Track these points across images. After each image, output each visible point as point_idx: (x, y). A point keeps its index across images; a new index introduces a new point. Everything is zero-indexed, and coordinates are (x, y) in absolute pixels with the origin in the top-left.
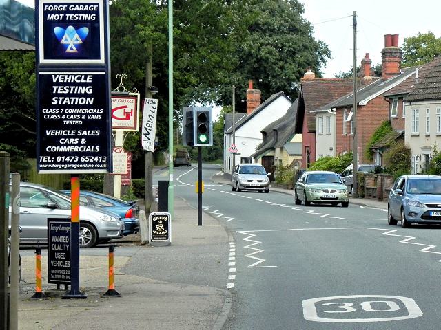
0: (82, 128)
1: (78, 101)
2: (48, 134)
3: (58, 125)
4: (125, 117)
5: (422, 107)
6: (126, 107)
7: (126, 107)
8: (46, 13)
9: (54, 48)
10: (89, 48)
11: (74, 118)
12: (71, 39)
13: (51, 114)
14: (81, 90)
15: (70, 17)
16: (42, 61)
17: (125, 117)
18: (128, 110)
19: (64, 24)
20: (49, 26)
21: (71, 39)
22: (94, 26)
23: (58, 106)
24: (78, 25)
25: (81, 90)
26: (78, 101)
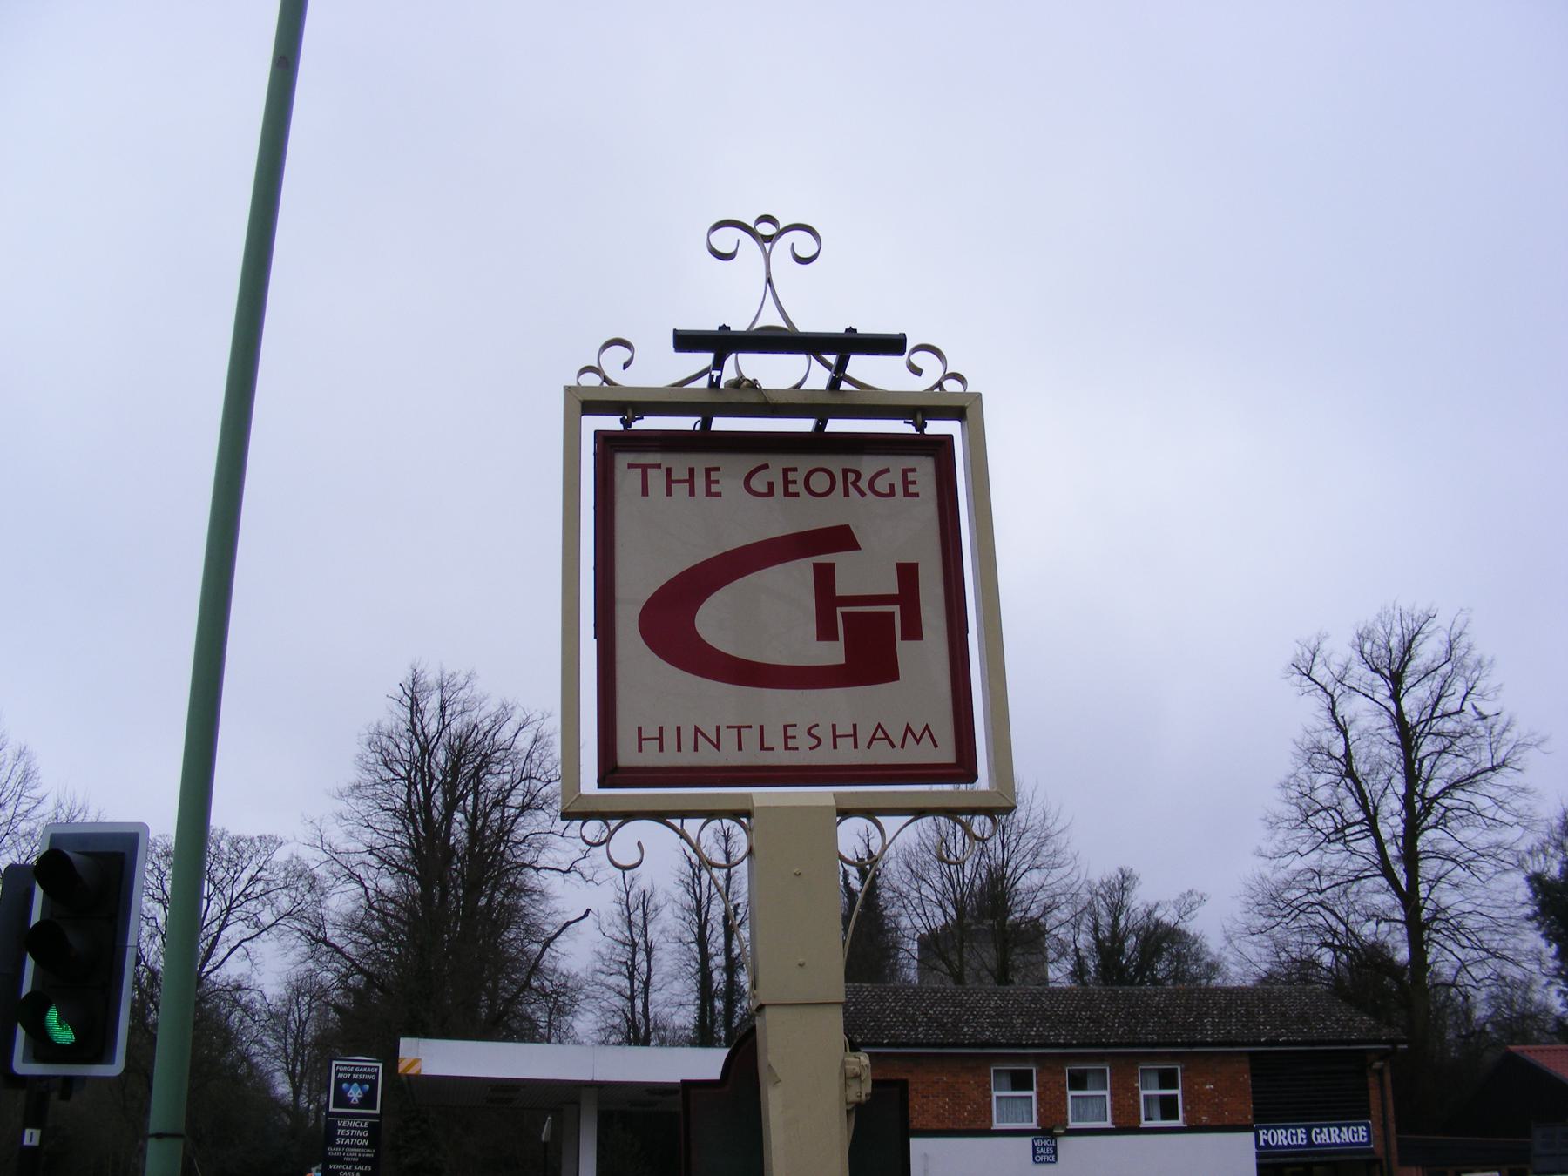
0: (358, 1163)
1: (357, 1142)
2: (1362, 1131)
3: (339, 1160)
4: (833, 653)
5: (913, 1114)
6: (842, 539)
7: (842, 539)
8: (337, 1072)
9: (342, 1100)
10: (367, 1100)
11: (353, 1155)
12: (355, 1093)
13: (334, 1152)
14: (359, 1133)
15: (356, 1076)
16: (331, 1109)
17: (833, 653)
18: (863, 575)
19: (351, 1081)
20: (339, 1082)
21: (355, 1093)
22: (373, 1084)
23: (341, 1146)
24: (361, 1082)
25: (359, 1133)
26: (357, 1142)
